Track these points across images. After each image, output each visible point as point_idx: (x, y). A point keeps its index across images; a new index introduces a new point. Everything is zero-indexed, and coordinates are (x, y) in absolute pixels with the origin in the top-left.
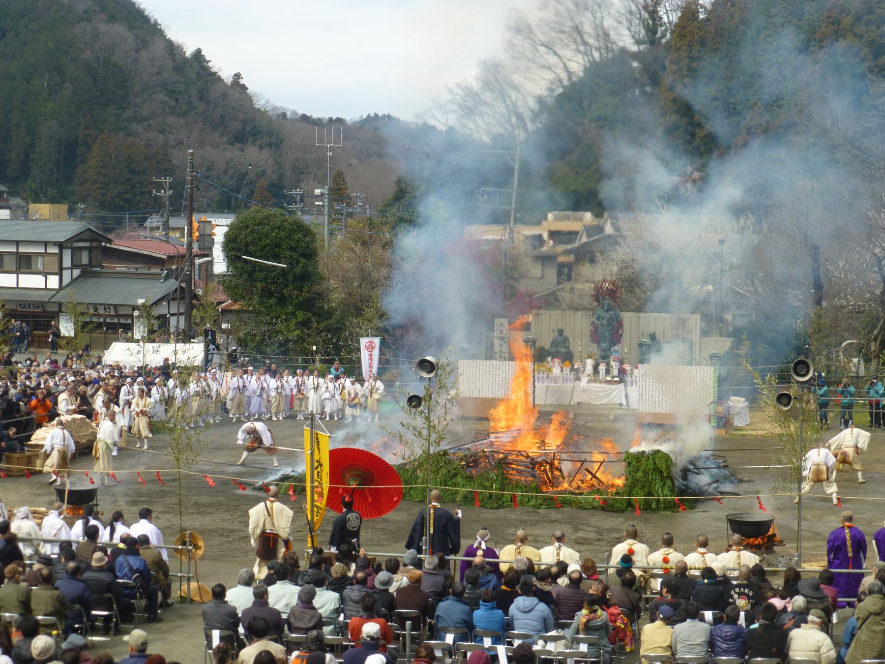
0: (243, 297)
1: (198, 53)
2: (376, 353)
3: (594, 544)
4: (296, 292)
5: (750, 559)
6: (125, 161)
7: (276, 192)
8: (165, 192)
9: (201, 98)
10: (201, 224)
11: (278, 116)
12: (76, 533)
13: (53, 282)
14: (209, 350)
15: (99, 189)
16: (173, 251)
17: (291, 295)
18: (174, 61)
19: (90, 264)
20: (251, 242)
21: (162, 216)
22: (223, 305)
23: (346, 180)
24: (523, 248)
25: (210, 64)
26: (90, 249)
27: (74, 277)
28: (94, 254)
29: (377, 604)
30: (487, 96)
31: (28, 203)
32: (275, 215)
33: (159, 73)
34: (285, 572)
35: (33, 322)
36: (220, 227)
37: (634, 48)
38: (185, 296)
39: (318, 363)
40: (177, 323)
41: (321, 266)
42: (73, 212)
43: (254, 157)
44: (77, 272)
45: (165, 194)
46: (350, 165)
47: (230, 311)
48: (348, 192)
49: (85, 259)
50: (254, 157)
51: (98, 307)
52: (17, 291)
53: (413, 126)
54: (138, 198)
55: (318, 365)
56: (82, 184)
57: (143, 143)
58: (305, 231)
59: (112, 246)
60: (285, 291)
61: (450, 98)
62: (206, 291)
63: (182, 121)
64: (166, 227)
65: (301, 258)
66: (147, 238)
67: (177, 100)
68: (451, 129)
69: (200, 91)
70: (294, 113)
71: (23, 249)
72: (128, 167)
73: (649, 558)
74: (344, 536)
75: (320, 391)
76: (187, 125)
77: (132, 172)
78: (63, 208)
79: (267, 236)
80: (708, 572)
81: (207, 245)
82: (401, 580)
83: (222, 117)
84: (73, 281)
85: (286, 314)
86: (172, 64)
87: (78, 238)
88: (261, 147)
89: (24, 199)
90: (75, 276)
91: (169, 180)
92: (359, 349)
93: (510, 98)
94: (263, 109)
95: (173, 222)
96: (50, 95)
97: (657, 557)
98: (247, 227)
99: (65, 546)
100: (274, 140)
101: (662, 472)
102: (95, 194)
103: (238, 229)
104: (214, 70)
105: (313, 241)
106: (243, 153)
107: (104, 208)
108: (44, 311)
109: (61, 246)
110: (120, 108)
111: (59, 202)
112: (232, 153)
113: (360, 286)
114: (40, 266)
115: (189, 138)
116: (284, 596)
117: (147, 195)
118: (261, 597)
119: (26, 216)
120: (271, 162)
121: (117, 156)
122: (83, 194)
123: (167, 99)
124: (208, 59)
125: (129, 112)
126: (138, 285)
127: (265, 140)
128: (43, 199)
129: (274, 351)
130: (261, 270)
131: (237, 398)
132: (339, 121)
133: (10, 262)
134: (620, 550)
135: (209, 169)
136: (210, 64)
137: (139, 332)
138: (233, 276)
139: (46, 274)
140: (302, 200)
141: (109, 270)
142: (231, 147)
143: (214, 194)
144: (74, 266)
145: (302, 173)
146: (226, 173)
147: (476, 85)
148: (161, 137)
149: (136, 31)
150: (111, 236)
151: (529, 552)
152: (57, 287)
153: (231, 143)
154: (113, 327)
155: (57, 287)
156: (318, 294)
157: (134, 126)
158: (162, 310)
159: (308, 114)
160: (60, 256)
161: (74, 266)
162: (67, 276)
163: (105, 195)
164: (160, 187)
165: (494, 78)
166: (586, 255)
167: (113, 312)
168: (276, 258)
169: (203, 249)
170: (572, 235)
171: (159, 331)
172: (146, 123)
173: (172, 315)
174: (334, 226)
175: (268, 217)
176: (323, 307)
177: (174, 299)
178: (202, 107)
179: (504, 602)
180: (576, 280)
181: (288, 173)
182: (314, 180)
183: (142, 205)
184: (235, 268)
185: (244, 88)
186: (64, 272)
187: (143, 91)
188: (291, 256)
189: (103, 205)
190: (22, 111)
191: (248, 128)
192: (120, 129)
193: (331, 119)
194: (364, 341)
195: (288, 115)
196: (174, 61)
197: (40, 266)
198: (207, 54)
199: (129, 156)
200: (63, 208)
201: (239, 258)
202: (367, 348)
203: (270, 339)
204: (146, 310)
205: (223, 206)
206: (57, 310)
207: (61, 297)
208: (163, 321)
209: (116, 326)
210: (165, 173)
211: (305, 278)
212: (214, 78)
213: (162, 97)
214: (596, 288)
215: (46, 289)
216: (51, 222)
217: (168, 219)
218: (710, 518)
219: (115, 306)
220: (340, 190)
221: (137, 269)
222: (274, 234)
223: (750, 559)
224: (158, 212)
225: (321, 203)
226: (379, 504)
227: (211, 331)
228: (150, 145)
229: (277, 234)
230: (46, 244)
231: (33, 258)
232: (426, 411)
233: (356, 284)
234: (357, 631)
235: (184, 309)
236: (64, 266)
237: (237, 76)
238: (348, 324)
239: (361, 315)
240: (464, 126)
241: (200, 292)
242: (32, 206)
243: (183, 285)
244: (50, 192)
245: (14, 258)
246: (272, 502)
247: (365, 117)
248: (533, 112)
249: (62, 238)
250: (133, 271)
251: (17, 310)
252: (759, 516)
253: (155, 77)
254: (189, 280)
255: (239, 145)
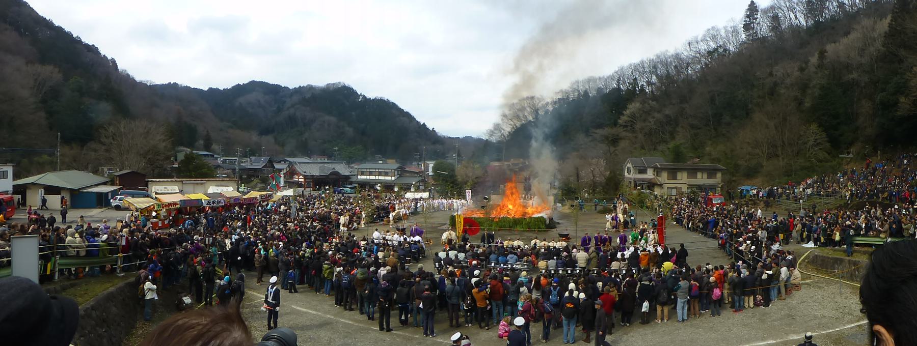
3: (527, 241)
5: (565, 244)
12: (402, 239)
13: (393, 178)
24: (505, 167)
28: (402, 172)
29: (476, 256)
34: (452, 249)
36: (431, 165)
38: (424, 182)
40: (422, 187)
43: (439, 147)
50: (439, 147)
66: (413, 167)
73: (540, 244)
74: (465, 240)
75: (456, 203)
80: (555, 248)
82: (480, 251)
97: (542, 243)
99: (400, 242)
116: (452, 254)
118: (447, 255)
134: (533, 242)
137: (413, 190)
151: (511, 243)
165: (497, 127)
166: (522, 169)
170: (517, 164)
179: (506, 256)
209: (408, 189)
218: (554, 232)
223: (565, 244)
226: (473, 232)
234: (471, 263)
235: (423, 184)
252: (566, 233)
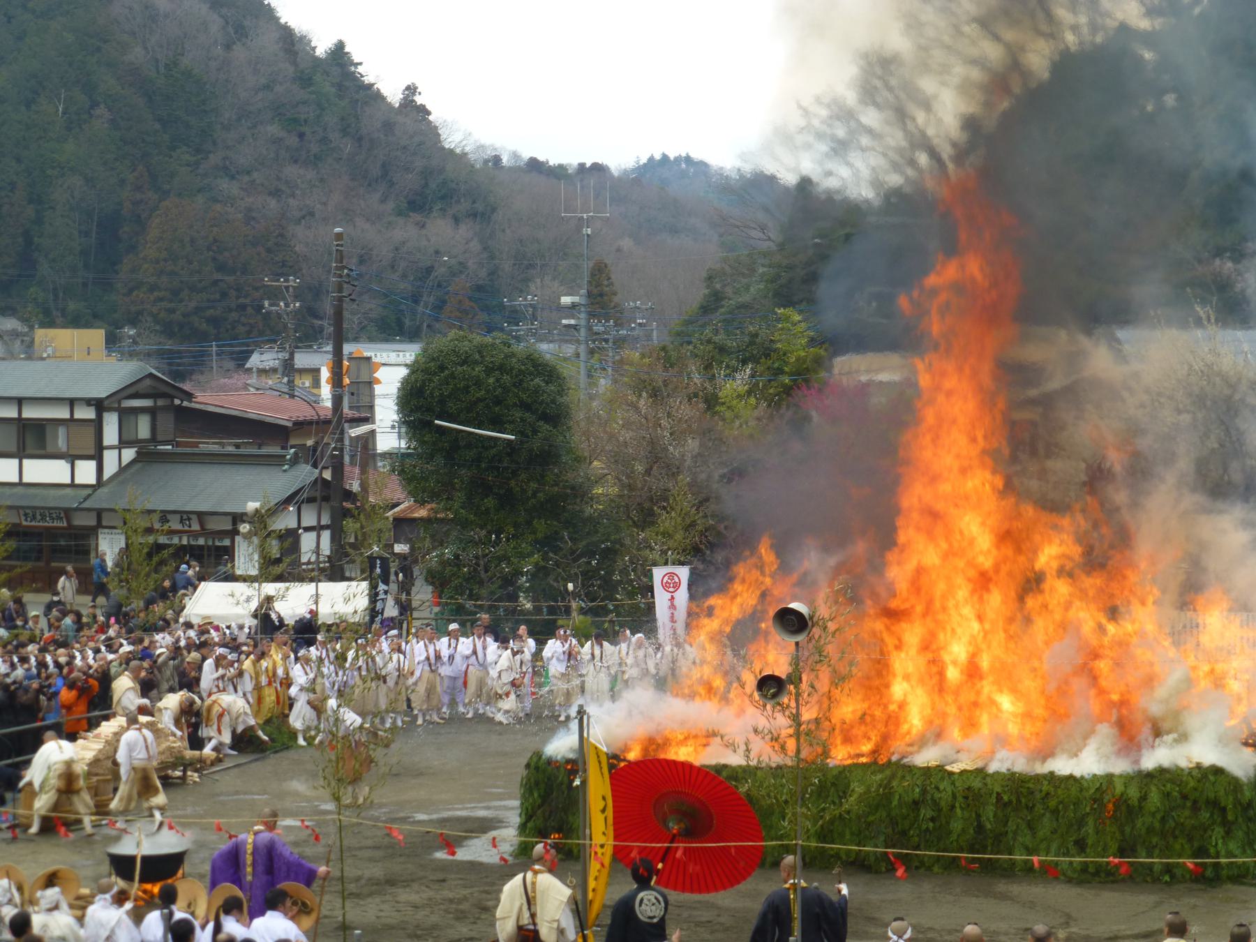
0: (434, 496)
1: (339, 51)
2: (682, 595)
4: (534, 485)
6: (209, 249)
7: (487, 300)
8: (287, 305)
9: (345, 131)
10: (354, 363)
11: (486, 162)
13: (86, 472)
14: (377, 594)
15: (161, 299)
16: (306, 413)
17: (524, 491)
18: (295, 64)
19: (154, 439)
20: (449, 396)
21: (282, 349)
22: (396, 510)
23: (613, 277)
25: (360, 69)
26: (152, 411)
27: (124, 463)
28: (176, 424)
30: (871, 117)
31: (32, 328)
32: (493, 345)
33: (267, 87)
35: (46, 542)
36: (391, 368)
37: (1144, 24)
38: (331, 497)
39: (574, 614)
41: (576, 438)
42: (114, 343)
43: (444, 237)
44: (129, 454)
45: (287, 307)
46: (619, 250)
47: (413, 520)
48: (616, 299)
49: (143, 429)
50: (444, 237)
51: (169, 517)
52: (20, 490)
53: (734, 175)
54: (234, 315)
55: (577, 618)
56: (131, 291)
57: (240, 216)
58: (549, 373)
59: (193, 405)
60: (513, 483)
61: (802, 123)
62: (364, 486)
63: (311, 174)
64: (288, 368)
65: (541, 423)
66: (246, 388)
67: (301, 136)
68: (805, 184)
69: (343, 119)
70: (515, 155)
71: (30, 413)
72: (214, 259)
76: (322, 180)
77: (221, 268)
78: (97, 336)
79: (478, 383)
81: (364, 400)
83: (383, 165)
84: (122, 469)
85: (516, 525)
86: (291, 69)
87: (131, 390)
88: (456, 220)
89: (24, 320)
90: (125, 461)
91: (293, 281)
92: (651, 589)
93: (914, 119)
94: (458, 151)
95: (302, 360)
96: (69, 129)
98: (442, 368)
100: (480, 207)
101: (1224, 810)
102: (155, 310)
103: (426, 371)
104: (367, 80)
105: (561, 392)
106: (424, 232)
107: (171, 335)
108: (70, 526)
109: (100, 406)
110: (198, 151)
111: (88, 325)
112: (405, 232)
113: (648, 472)
114: (62, 444)
115: (325, 204)
117: (250, 310)
119: (30, 353)
120: (475, 246)
121: (192, 241)
122: (133, 309)
123: (283, 134)
124: (356, 59)
125: (214, 159)
126: (240, 477)
127: (465, 206)
128: (59, 320)
129: (493, 593)
130: (469, 446)
131: (425, 679)
132: (598, 168)
133: (8, 439)
135: (362, 261)
136: (360, 69)
137: (246, 559)
138: (420, 456)
139: (72, 458)
140: (534, 318)
141: (189, 450)
142: (401, 221)
143: (372, 306)
144: (123, 443)
145: (531, 266)
146: (393, 267)
147: (850, 97)
148: (273, 203)
149: (224, 11)
150: (187, 386)
152: (93, 481)
153: (400, 214)
154: (196, 553)
155: (93, 481)
156: (573, 488)
157: (224, 185)
158: (287, 521)
159: (541, 158)
160: (98, 425)
161: (123, 443)
162: (111, 463)
163: (172, 311)
164: (275, 295)
167: (196, 527)
168: (497, 424)
169: (358, 408)
171: (283, 564)
172: (246, 178)
173: (307, 529)
174: (594, 361)
175: (480, 349)
176: (582, 511)
177: (310, 500)
178: (348, 147)
180: (1048, 455)
181: (507, 266)
182: (554, 279)
183: (241, 329)
184: (422, 443)
185: (424, 111)
186: (106, 453)
187: (239, 119)
188: (522, 420)
189: (168, 330)
190: (19, 160)
191: (433, 185)
192: (199, 191)
193: (582, 166)
194: (658, 573)
195: (505, 159)
196: (295, 64)
197: (62, 444)
198: (355, 51)
199: (215, 241)
200: (97, 336)
201: (430, 423)
202: (665, 586)
203: (486, 571)
204: (260, 519)
205: (392, 329)
206: (93, 523)
207: (101, 500)
208: (290, 539)
210: (285, 269)
211: (547, 457)
212: (370, 95)
213: (273, 129)
214: (1089, 467)
215: (73, 485)
216: (79, 363)
217: (292, 354)
219: (201, 515)
220: (601, 295)
221: (237, 446)
222: (491, 380)
224: (275, 341)
225: (572, 322)
227: (381, 558)
228: (254, 218)
229: (498, 380)
230: (72, 402)
231: (49, 430)
232: (793, 704)
233: (639, 468)
236: (106, 443)
237: (411, 90)
238: (628, 541)
239: (653, 523)
240: (829, 174)
241: (355, 487)
242: (40, 334)
243: (327, 475)
244: (72, 306)
245: (13, 430)
246: (536, 873)
247: (644, 160)
248: (954, 145)
249: (101, 392)
250: (231, 449)
251: (19, 525)
253: (260, 95)
254: (338, 468)
255: (416, 217)
